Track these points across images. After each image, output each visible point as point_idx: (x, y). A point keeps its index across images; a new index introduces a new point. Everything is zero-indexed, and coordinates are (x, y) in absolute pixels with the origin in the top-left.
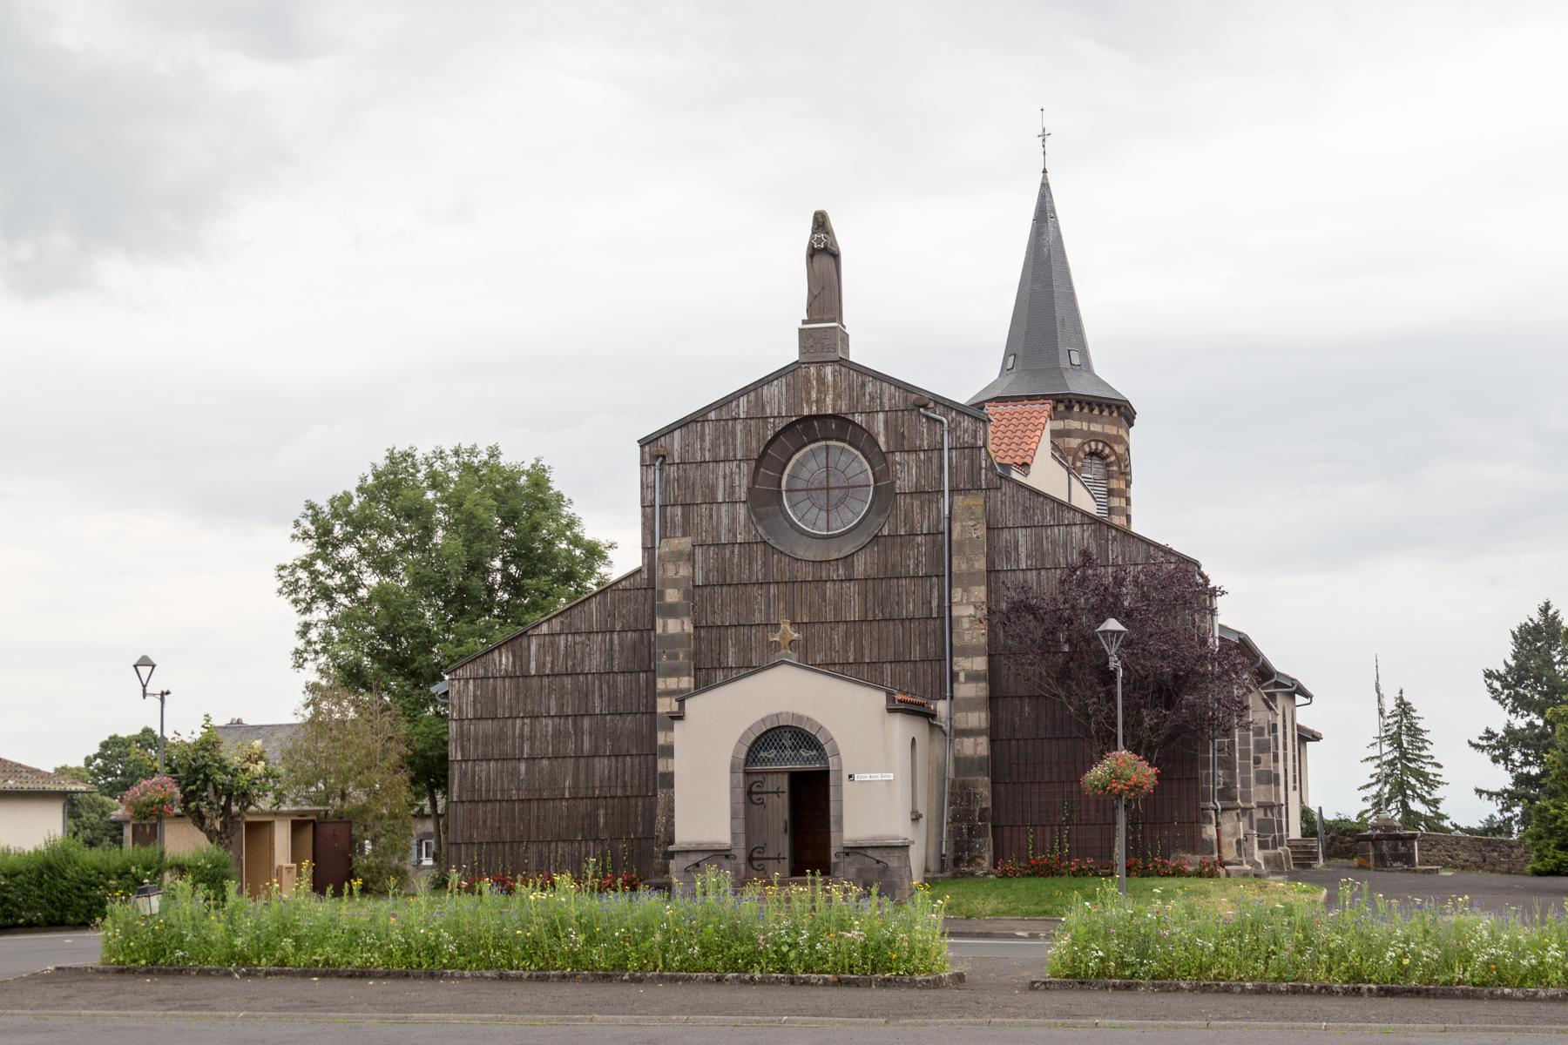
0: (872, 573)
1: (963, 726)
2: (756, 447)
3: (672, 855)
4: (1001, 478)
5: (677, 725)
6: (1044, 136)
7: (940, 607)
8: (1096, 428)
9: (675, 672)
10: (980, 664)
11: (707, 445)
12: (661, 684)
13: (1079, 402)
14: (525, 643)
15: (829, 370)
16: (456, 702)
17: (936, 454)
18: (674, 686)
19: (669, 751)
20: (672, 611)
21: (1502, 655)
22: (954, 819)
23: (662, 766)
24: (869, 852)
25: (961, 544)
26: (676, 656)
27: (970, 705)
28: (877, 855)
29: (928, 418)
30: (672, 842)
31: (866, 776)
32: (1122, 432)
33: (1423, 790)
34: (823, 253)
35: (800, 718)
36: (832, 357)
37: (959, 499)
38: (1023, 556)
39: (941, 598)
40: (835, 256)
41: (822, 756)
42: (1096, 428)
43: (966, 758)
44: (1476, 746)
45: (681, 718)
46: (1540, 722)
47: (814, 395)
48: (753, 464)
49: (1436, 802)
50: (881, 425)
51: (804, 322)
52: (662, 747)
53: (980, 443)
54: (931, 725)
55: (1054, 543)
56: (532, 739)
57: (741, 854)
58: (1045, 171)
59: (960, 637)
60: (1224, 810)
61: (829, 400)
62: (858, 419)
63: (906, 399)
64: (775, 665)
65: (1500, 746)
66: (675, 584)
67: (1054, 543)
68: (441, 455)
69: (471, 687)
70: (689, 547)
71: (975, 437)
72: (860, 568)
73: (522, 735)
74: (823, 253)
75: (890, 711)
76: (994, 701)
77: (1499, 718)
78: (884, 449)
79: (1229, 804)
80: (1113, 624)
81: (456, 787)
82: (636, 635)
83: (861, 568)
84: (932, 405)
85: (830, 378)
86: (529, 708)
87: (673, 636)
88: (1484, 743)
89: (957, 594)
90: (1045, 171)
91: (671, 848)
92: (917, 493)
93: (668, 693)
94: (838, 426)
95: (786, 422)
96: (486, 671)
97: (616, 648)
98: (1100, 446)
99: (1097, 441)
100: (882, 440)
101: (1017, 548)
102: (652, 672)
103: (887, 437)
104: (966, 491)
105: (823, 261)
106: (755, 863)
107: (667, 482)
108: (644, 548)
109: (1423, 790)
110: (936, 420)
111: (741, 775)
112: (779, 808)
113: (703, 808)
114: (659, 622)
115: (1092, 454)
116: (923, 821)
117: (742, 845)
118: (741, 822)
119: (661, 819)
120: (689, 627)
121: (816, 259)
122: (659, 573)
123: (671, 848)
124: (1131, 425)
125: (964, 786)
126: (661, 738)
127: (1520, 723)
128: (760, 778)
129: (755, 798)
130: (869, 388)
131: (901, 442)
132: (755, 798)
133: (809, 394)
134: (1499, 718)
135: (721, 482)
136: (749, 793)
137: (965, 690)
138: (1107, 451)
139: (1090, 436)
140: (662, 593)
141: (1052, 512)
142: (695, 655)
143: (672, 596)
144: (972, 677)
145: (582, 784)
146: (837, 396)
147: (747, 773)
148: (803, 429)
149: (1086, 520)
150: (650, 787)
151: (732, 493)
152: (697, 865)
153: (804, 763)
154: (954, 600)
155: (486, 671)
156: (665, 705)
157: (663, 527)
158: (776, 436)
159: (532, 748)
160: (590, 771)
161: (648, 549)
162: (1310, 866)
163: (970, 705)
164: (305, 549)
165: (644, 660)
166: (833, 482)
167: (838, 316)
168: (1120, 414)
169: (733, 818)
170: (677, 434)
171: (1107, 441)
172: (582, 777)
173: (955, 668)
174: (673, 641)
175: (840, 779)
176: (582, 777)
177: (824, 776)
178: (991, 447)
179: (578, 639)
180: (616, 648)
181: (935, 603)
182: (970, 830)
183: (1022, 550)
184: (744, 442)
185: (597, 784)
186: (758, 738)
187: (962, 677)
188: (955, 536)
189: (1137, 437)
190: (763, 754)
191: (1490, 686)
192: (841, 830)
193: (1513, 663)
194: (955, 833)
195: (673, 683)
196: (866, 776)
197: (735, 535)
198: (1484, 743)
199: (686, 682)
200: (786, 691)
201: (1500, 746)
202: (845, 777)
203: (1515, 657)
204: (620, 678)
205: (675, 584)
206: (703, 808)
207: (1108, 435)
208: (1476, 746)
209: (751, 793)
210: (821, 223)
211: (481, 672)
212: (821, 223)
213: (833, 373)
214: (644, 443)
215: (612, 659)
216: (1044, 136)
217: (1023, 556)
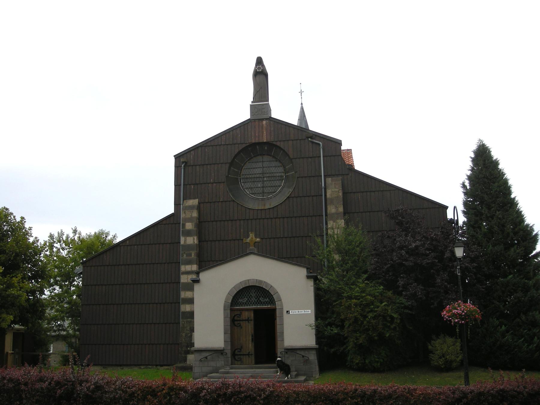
3: (188, 352)
5: (196, 287)
6: (301, 92)
9: (189, 263)
19: (191, 301)
20: (188, 233)
24: (298, 352)
26: (191, 255)
28: (302, 353)
29: (313, 142)
31: (296, 312)
34: (260, 74)
35: (261, 282)
37: (329, 180)
40: (266, 75)
48: (228, 165)
52: (183, 299)
57: (229, 352)
58: (302, 104)
66: (190, 220)
70: (197, 203)
74: (260, 74)
84: (314, 137)
87: (189, 245)
90: (302, 104)
95: (244, 146)
102: (178, 264)
105: (262, 77)
106: (236, 357)
111: (229, 311)
112: (249, 328)
113: (209, 329)
117: (229, 347)
118: (229, 336)
120: (196, 242)
121: (258, 77)
140: (184, 225)
142: (199, 255)
143: (189, 226)
152: (206, 358)
156: (184, 279)
158: (239, 153)
161: (177, 204)
167: (268, 100)
169: (225, 333)
174: (188, 247)
175: (282, 313)
177: (274, 311)
190: (240, 300)
192: (283, 340)
195: (188, 268)
196: (296, 312)
199: (195, 267)
202: (285, 312)
205: (190, 220)
206: (209, 329)
209: (234, 319)
210: (259, 61)
212: (259, 61)
216: (301, 92)
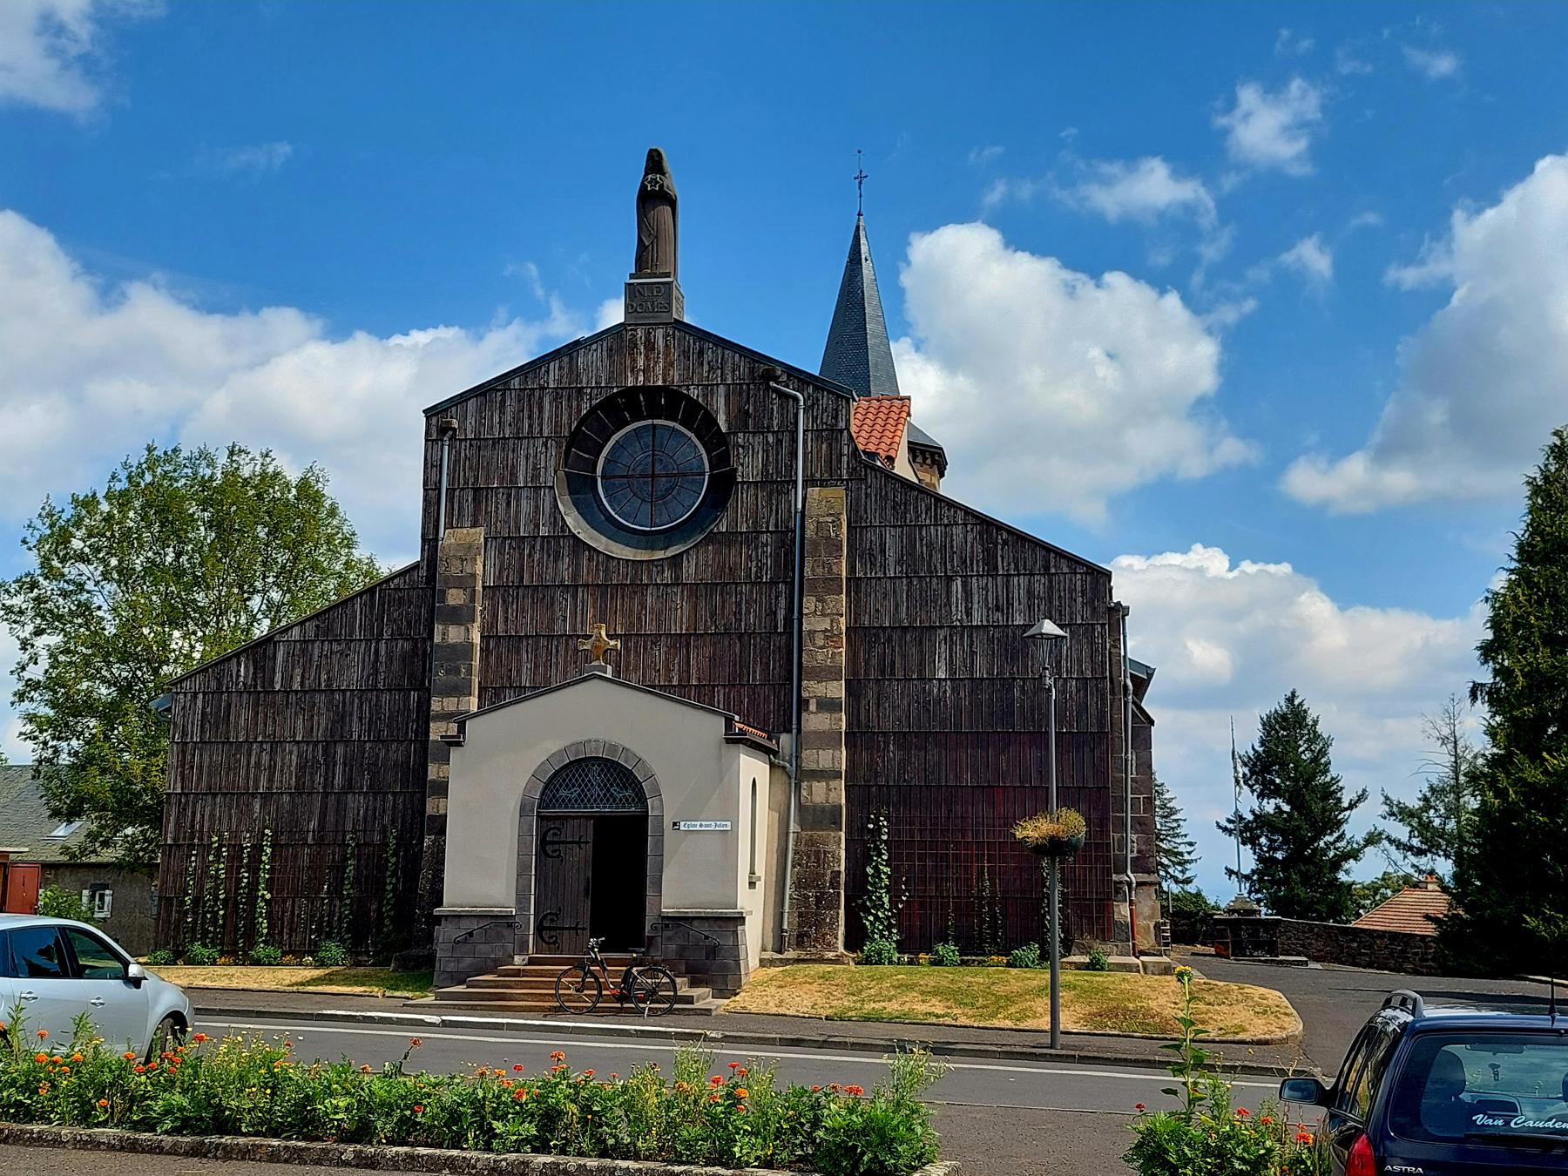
0: (708, 577)
1: (814, 767)
2: (568, 423)
4: (866, 467)
5: (455, 753)
7: (788, 620)
10: (837, 690)
11: (508, 417)
12: (436, 705)
14: (270, 652)
15: (660, 333)
16: (179, 720)
17: (786, 438)
18: (452, 708)
19: (442, 789)
21: (1250, 738)
22: (798, 885)
23: (431, 807)
25: (815, 544)
27: (827, 740)
28: (705, 929)
29: (781, 394)
30: (440, 904)
32: (935, 480)
33: (1175, 871)
35: (613, 748)
36: (664, 318)
37: (814, 492)
38: (891, 561)
39: (790, 609)
41: (641, 799)
43: (815, 807)
44: (1225, 829)
45: (459, 744)
46: (1286, 808)
47: (641, 362)
49: (1188, 881)
50: (722, 400)
53: (842, 425)
54: (772, 765)
55: (930, 545)
56: (272, 769)
59: (811, 654)
60: (1139, 884)
62: (694, 393)
63: (752, 371)
64: (585, 680)
65: (1247, 830)
67: (930, 545)
68: (203, 455)
69: (199, 703)
71: (836, 418)
72: (689, 571)
73: (258, 764)
75: (728, 741)
76: (855, 738)
77: (1249, 803)
78: (724, 430)
80: (1049, 627)
81: (171, 826)
82: (407, 645)
83: (692, 570)
85: (661, 342)
86: (270, 730)
87: (454, 646)
88: (1231, 826)
89: (810, 604)
91: (437, 911)
92: (764, 482)
93: (447, 717)
94: (667, 401)
96: (220, 684)
97: (383, 659)
101: (883, 551)
103: (728, 414)
104: (823, 483)
107: (457, 461)
108: (424, 539)
109: (1175, 871)
110: (788, 396)
112: (579, 859)
113: (483, 861)
114: (438, 628)
116: (760, 885)
119: (426, 874)
122: (441, 569)
123: (437, 911)
124: (942, 475)
125: (811, 842)
126: (433, 772)
127: (1269, 806)
128: (557, 824)
129: (549, 849)
131: (741, 420)
132: (549, 849)
133: (635, 360)
134: (1249, 803)
135: (523, 462)
136: (543, 843)
137: (815, 721)
141: (928, 509)
144: (828, 705)
145: (330, 826)
146: (669, 365)
147: (540, 817)
148: (623, 406)
149: (971, 520)
150: (417, 838)
151: (535, 477)
154: (805, 611)
155: (220, 684)
156: (437, 731)
157: (450, 515)
159: (271, 780)
160: (341, 809)
161: (430, 541)
163: (827, 740)
165: (418, 671)
166: (658, 469)
168: (934, 462)
170: (472, 404)
173: (805, 694)
178: (853, 429)
179: (335, 647)
180: (383, 659)
181: (781, 615)
182: (818, 900)
184: (554, 418)
185: (349, 827)
186: (557, 773)
187: (813, 707)
188: (809, 533)
190: (563, 793)
195: (450, 704)
197: (537, 526)
198: (1231, 826)
199: (473, 703)
200: (597, 713)
201: (1247, 830)
202: (667, 823)
203: (1262, 744)
204: (386, 697)
208: (1225, 829)
210: (655, 162)
211: (213, 685)
212: (655, 162)
213: (666, 336)
214: (430, 413)
215: (376, 672)
216: (861, 178)
217: (891, 561)
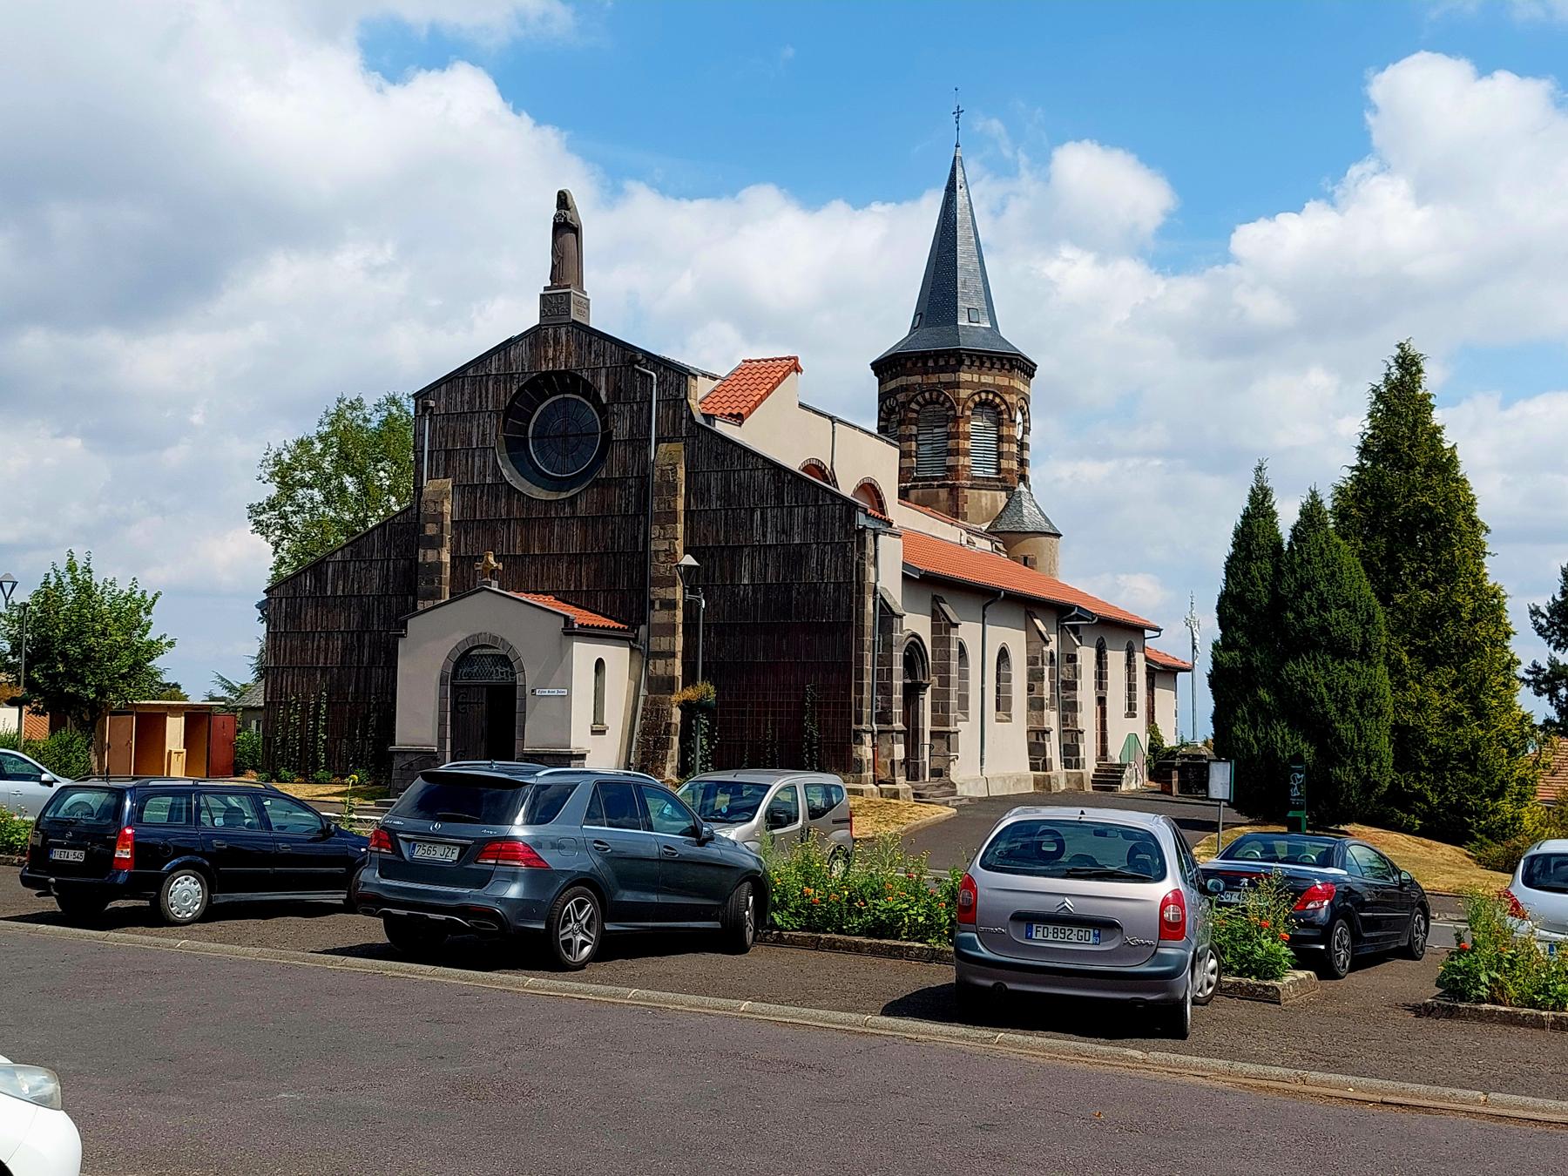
8: (986, 379)
11: (466, 397)
13: (970, 356)
34: (565, 228)
37: (662, 446)
42: (986, 379)
47: (550, 354)
51: (546, 289)
55: (739, 485)
60: (880, 732)
61: (563, 358)
63: (623, 356)
72: (582, 508)
74: (565, 228)
79: (885, 727)
88: (1530, 677)
94: (568, 381)
98: (983, 396)
99: (987, 392)
100: (603, 394)
113: (418, 718)
115: (982, 404)
130: (594, 347)
138: (997, 400)
139: (980, 388)
153: (497, 677)
162: (1111, 789)
164: (272, 490)
171: (998, 391)
172: (362, 685)
176: (362, 685)
177: (512, 688)
182: (655, 743)
183: (714, 491)
184: (495, 397)
189: (1035, 389)
191: (1535, 623)
193: (1559, 598)
194: (644, 744)
198: (1530, 677)
206: (418, 718)
207: (999, 387)
210: (563, 200)
215: (388, 583)
